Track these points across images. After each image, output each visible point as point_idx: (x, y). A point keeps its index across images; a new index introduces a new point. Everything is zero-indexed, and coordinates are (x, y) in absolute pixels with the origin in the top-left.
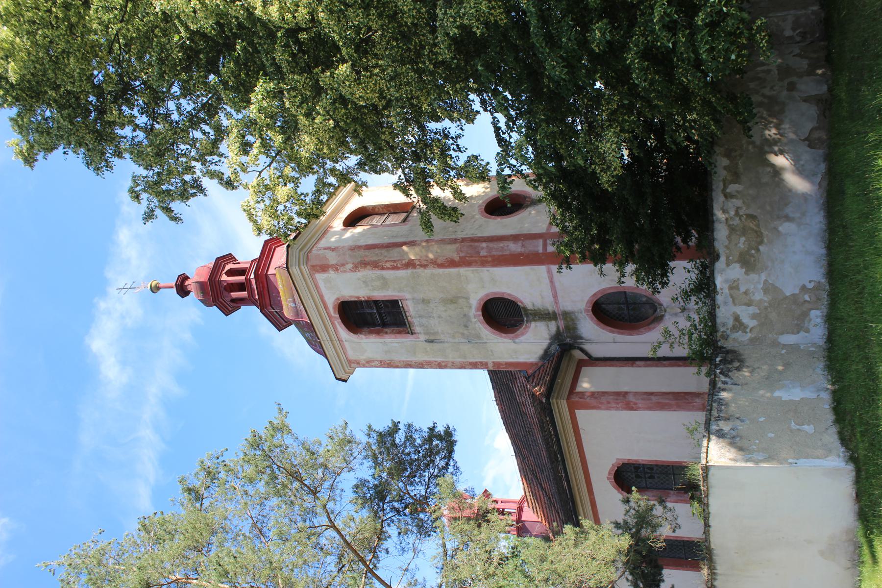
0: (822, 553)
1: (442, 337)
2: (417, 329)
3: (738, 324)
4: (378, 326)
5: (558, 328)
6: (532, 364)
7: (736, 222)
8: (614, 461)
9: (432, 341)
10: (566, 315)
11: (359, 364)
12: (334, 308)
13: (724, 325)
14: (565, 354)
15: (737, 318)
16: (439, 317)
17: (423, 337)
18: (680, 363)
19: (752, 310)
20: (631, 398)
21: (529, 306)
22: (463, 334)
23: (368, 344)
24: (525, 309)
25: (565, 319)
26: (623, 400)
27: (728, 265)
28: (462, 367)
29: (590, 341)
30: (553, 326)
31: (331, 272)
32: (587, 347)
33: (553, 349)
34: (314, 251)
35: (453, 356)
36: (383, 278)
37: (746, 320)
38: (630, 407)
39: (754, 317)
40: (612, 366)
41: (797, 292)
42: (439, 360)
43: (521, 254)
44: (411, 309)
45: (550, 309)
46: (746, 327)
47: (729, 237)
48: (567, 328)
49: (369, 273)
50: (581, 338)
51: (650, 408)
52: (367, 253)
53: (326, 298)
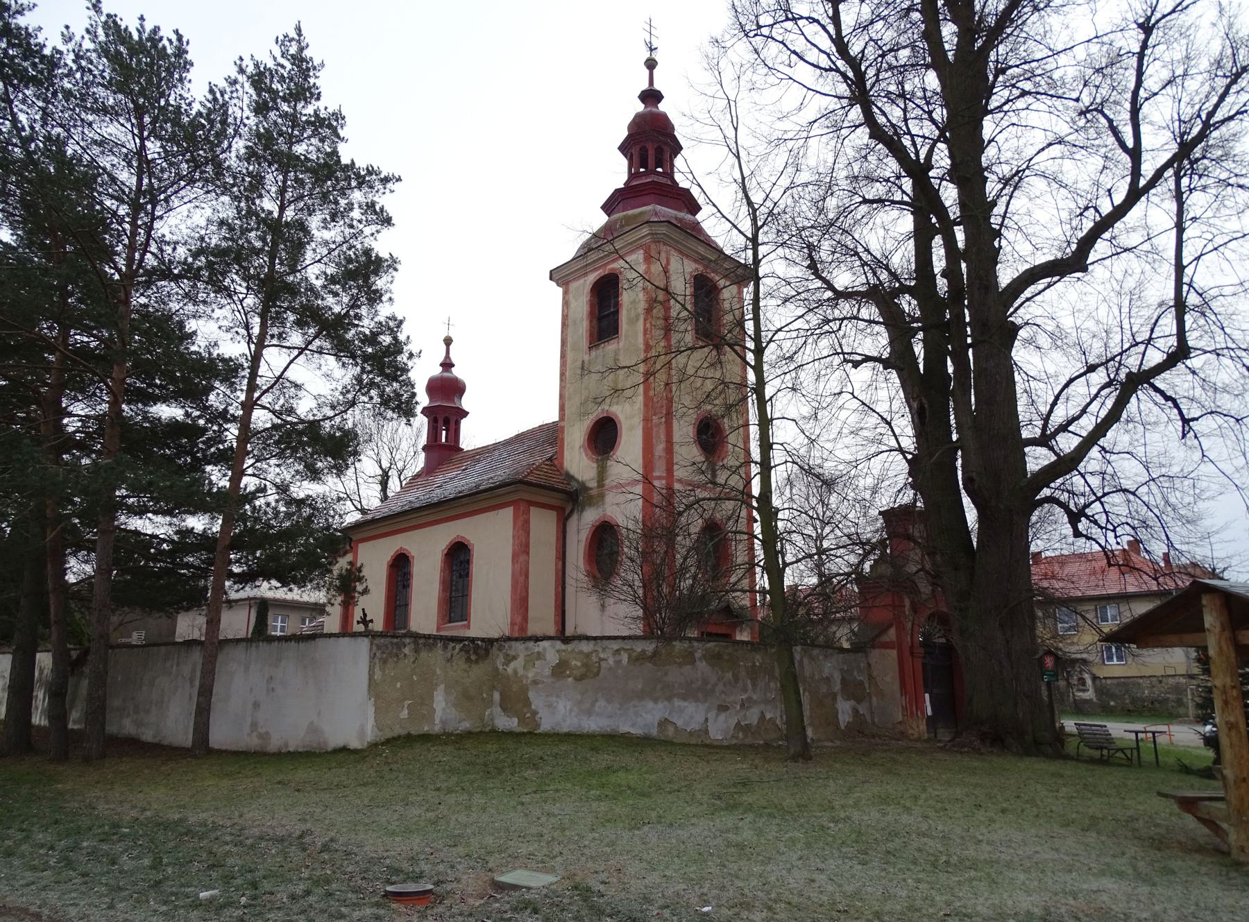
0: (312, 723)
2: (593, 353)
3: (510, 659)
6: (562, 464)
7: (594, 659)
9: (583, 368)
10: (602, 496)
11: (565, 293)
13: (510, 647)
14: (567, 498)
15: (514, 658)
17: (586, 358)
18: (560, 602)
19: (521, 672)
20: (522, 558)
23: (582, 305)
26: (522, 549)
28: (562, 397)
29: (579, 520)
30: (593, 484)
32: (575, 516)
34: (663, 248)
36: (637, 320)
37: (512, 665)
38: (515, 557)
39: (515, 672)
40: (558, 539)
43: (652, 453)
44: (610, 347)
45: (607, 482)
47: (581, 652)
48: (591, 497)
50: (582, 511)
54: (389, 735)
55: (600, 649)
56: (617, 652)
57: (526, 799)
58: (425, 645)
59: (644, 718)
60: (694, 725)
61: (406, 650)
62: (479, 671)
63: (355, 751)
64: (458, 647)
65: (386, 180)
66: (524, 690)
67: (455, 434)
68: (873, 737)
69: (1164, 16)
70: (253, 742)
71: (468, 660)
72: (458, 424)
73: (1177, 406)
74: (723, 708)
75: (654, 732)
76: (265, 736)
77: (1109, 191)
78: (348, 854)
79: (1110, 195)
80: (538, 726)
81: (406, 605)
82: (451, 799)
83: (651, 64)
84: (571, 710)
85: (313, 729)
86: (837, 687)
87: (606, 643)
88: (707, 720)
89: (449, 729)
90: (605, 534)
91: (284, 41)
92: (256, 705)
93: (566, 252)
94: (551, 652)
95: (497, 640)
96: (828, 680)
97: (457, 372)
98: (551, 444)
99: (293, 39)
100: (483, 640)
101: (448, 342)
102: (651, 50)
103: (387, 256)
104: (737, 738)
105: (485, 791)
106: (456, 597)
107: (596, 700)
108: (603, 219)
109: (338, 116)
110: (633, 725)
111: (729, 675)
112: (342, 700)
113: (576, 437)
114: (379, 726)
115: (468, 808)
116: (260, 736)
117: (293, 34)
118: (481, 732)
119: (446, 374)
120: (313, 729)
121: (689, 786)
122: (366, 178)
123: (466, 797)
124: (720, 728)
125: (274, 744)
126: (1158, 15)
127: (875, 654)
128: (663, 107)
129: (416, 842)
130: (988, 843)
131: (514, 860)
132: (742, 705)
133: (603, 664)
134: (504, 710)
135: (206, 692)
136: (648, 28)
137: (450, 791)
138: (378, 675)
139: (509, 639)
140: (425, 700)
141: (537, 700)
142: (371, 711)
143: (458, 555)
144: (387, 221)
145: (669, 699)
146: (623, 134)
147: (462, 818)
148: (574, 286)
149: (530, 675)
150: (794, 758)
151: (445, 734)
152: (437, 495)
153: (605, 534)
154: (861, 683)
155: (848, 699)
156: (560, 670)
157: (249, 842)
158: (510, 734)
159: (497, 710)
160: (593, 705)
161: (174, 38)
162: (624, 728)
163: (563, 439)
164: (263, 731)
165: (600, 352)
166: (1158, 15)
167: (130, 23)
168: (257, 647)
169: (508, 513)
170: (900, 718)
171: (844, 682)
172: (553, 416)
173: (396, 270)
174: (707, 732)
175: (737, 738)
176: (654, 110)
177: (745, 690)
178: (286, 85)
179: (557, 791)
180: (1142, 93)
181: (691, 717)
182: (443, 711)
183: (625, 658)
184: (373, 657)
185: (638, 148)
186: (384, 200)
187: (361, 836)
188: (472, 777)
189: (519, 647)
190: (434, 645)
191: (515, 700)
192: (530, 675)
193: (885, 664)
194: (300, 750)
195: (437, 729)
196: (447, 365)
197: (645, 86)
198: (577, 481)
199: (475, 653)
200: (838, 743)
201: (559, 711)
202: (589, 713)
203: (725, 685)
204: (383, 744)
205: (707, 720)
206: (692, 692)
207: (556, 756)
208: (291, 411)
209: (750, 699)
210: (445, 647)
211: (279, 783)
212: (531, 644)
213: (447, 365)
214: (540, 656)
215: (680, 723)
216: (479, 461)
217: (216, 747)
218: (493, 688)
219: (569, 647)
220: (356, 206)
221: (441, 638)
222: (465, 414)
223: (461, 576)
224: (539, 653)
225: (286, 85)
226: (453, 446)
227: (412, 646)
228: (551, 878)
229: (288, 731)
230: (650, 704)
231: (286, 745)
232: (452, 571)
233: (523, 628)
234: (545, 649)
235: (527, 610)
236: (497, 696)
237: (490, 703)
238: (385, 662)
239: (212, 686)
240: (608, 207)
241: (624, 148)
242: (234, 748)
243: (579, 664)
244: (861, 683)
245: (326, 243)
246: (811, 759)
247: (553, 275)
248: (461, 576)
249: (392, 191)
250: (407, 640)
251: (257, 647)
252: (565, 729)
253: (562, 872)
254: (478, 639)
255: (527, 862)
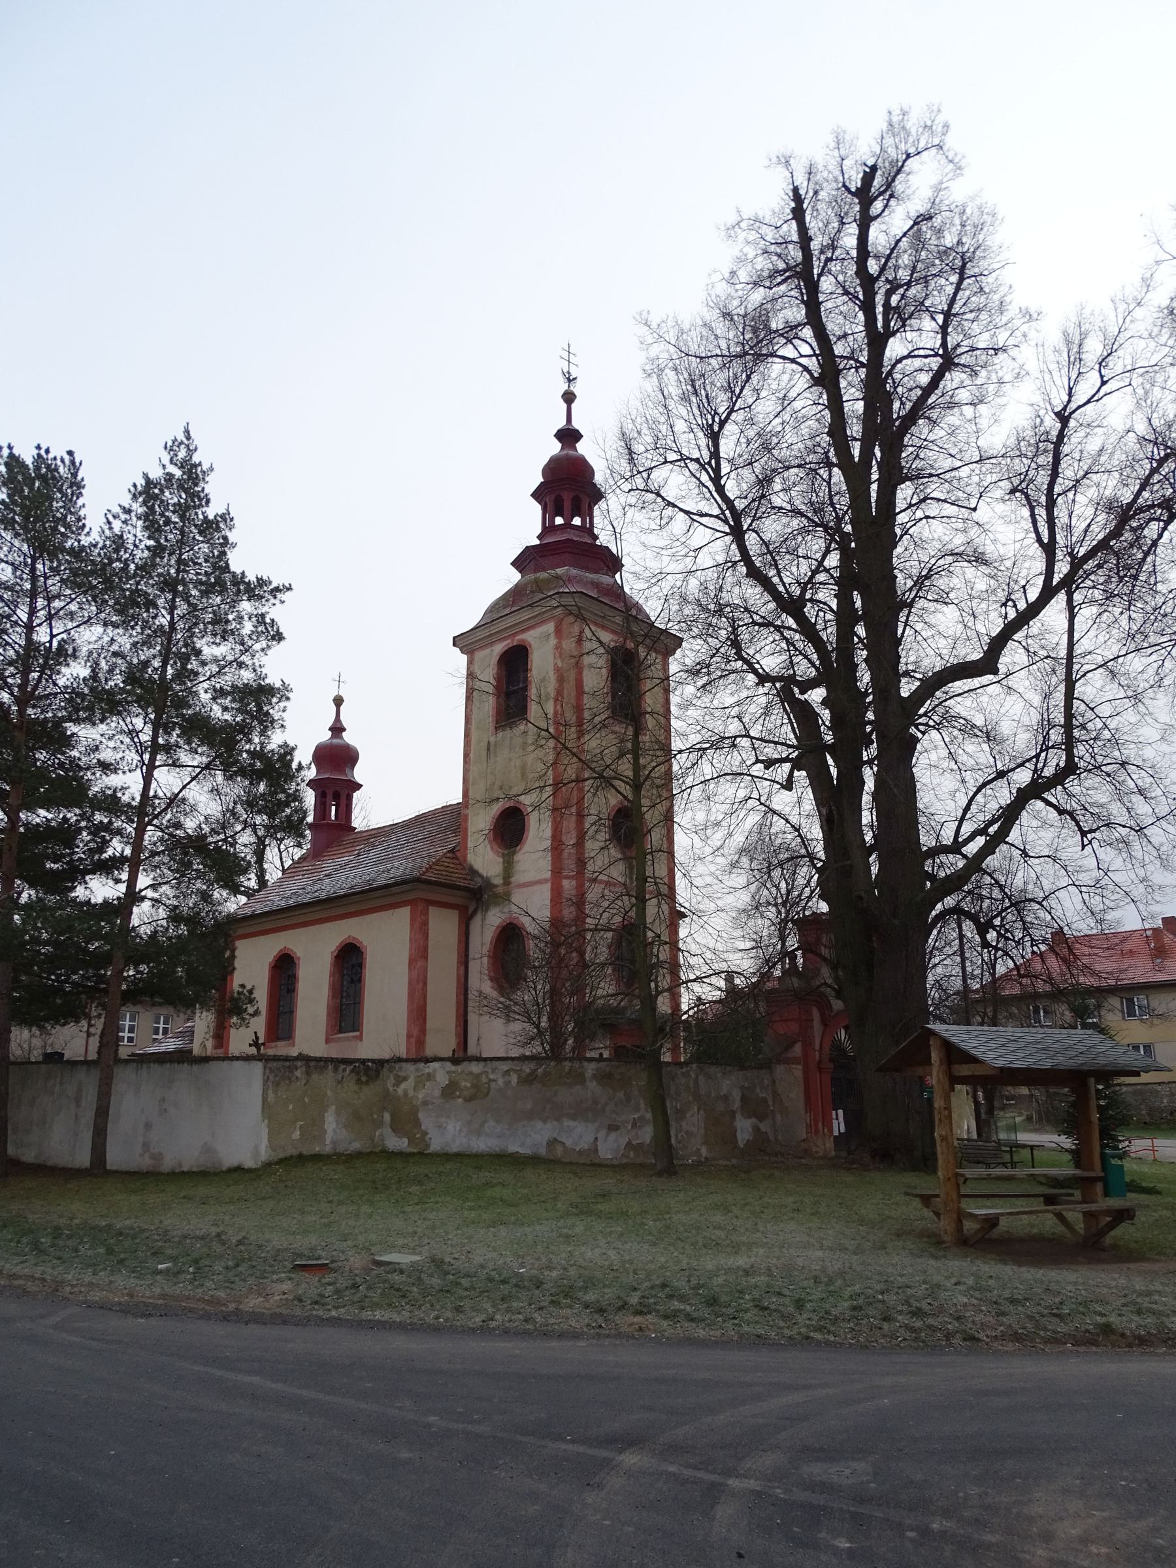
0: (206, 1143)
1: (492, 761)
2: (500, 734)
3: (400, 1080)
4: (507, 688)
5: (496, 886)
7: (484, 1079)
8: (365, 943)
9: (488, 749)
11: (470, 662)
12: (523, 640)
13: (401, 1068)
15: (405, 1079)
16: (510, 760)
18: (461, 1011)
19: (411, 1093)
20: (420, 964)
21: (516, 858)
22: (494, 784)
24: (514, 853)
25: (505, 893)
26: (420, 953)
27: (448, 1072)
31: (555, 642)
32: (479, 917)
33: (478, 880)
35: (473, 768)
37: (403, 1086)
38: (412, 962)
39: (406, 1092)
40: (459, 941)
41: (423, 1127)
42: (472, 755)
45: (513, 879)
46: (398, 1086)
47: (471, 1073)
48: (496, 896)
49: (551, 687)
50: (487, 910)
51: (410, 984)
52: (573, 683)
53: (531, 632)
54: (282, 1155)
55: (490, 1071)
56: (507, 1073)
57: (409, 1209)
58: (316, 1067)
59: (532, 1138)
60: (584, 1145)
61: (298, 1073)
62: (370, 1092)
63: (250, 1171)
64: (349, 1069)
65: (277, 589)
66: (414, 1112)
67: (346, 810)
68: (776, 1155)
69: (1079, 407)
70: (145, 1163)
71: (359, 1082)
72: (349, 798)
73: (1073, 819)
74: (613, 1128)
75: (543, 1151)
76: (158, 1157)
77: (1024, 587)
78: (260, 1247)
79: (1025, 592)
80: (428, 1146)
81: (291, 1012)
82: (342, 1209)
83: (569, 398)
84: (461, 1131)
85: (207, 1149)
86: (737, 1105)
87: (496, 1064)
88: (596, 1139)
89: (340, 1149)
90: (510, 935)
91: (171, 448)
92: (148, 1126)
93: (470, 619)
94: (441, 1073)
95: (387, 1061)
96: (726, 1098)
97: (348, 737)
98: (454, 831)
99: (182, 443)
100: (373, 1061)
101: (338, 701)
102: (569, 380)
103: (278, 684)
104: (627, 1157)
105: (371, 1202)
106: (346, 1011)
107: (485, 1121)
108: (515, 576)
109: (226, 518)
110: (522, 1145)
111: (621, 1095)
112: (238, 1122)
113: (481, 821)
114: (272, 1147)
115: (357, 1215)
116: (153, 1157)
117: (181, 437)
118: (371, 1153)
119: (336, 741)
120: (207, 1149)
121: (555, 1199)
122: (258, 590)
123: (355, 1207)
124: (610, 1147)
125: (168, 1164)
126: (1073, 406)
127: (780, 1070)
128: (582, 448)
129: (313, 1239)
130: (847, 1249)
131: (392, 1248)
132: (634, 1125)
133: (493, 1085)
134: (394, 1131)
135: (102, 1113)
136: (565, 355)
137: (341, 1203)
138: (271, 1097)
139: (400, 1060)
140: (317, 1122)
141: (427, 1121)
142: (265, 1132)
143: (349, 959)
144: (279, 637)
145: (558, 1119)
146: (537, 479)
147: (351, 1222)
148: (479, 655)
149: (420, 1096)
150: (660, 1174)
151: (336, 1154)
152: (328, 888)
153: (510, 935)
154: (765, 1100)
155: (749, 1117)
156: (449, 1091)
157: (177, 1239)
158: (400, 1154)
159: (387, 1131)
160: (482, 1125)
161: (67, 458)
162: (513, 1148)
163: (466, 829)
164: (156, 1151)
165: (508, 733)
166: (1073, 406)
167: (28, 456)
168: (149, 1068)
169: (405, 912)
170: (805, 1136)
171: (744, 1099)
172: (456, 797)
173: (288, 699)
174: (596, 1151)
175: (627, 1157)
176: (571, 452)
177: (637, 1109)
178: (177, 500)
179: (437, 1203)
180: (1057, 489)
181: (581, 1137)
182: (334, 1132)
183: (514, 1079)
184: (266, 1081)
185: (553, 496)
186: (275, 611)
187: (267, 1236)
188: (361, 1192)
189: (410, 1068)
190: (325, 1067)
191: (406, 1121)
192: (420, 1096)
193: (790, 1082)
194: (195, 1169)
195: (328, 1149)
196: (337, 729)
197: (562, 423)
198: (481, 876)
199: (366, 1074)
200: (734, 1161)
201: (448, 1132)
202: (479, 1133)
203: (616, 1105)
204: (277, 1163)
205: (596, 1139)
206: (580, 1112)
207: (440, 1174)
208: (178, 825)
209: (642, 1118)
210: (336, 1069)
211: (184, 1197)
212: (421, 1065)
213: (337, 729)
214: (430, 1077)
215: (569, 1143)
216: (374, 846)
217: (114, 1168)
218: (384, 1108)
219: (459, 1068)
220: (246, 617)
221: (332, 1060)
222: (358, 786)
223: (352, 981)
224: (429, 1074)
225: (177, 500)
226: (344, 824)
227: (304, 1069)
228: (417, 1258)
229: (182, 1148)
230: (539, 1125)
231: (180, 1165)
232: (342, 976)
233: (420, 1043)
234: (435, 1071)
235: (425, 1019)
236: (387, 1117)
237: (380, 1124)
238: (277, 1085)
239: (108, 1107)
240: (519, 563)
241: (537, 495)
242: (125, 1168)
243: (469, 1085)
244: (765, 1100)
245: (216, 660)
246: (676, 1173)
247: (456, 641)
248: (352, 981)
249: (282, 602)
250: (299, 1063)
251: (149, 1068)
252: (455, 1149)
253: (425, 1254)
254: (369, 1060)
255: (401, 1249)
